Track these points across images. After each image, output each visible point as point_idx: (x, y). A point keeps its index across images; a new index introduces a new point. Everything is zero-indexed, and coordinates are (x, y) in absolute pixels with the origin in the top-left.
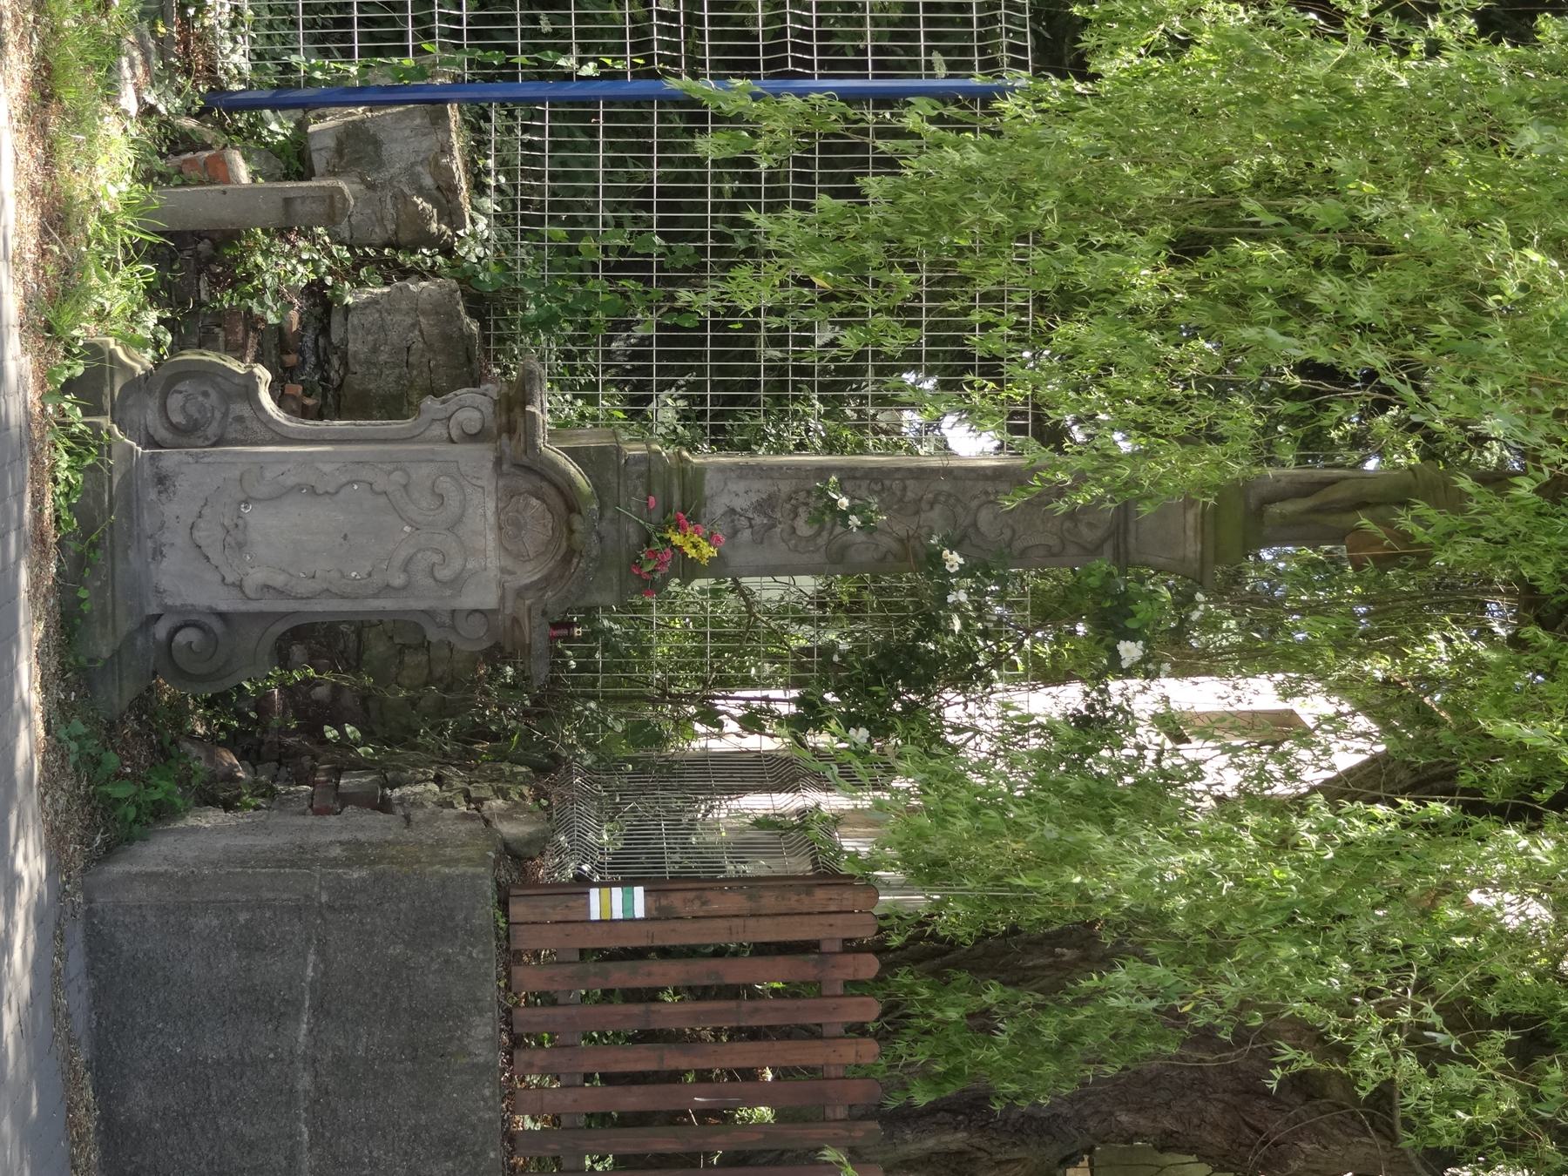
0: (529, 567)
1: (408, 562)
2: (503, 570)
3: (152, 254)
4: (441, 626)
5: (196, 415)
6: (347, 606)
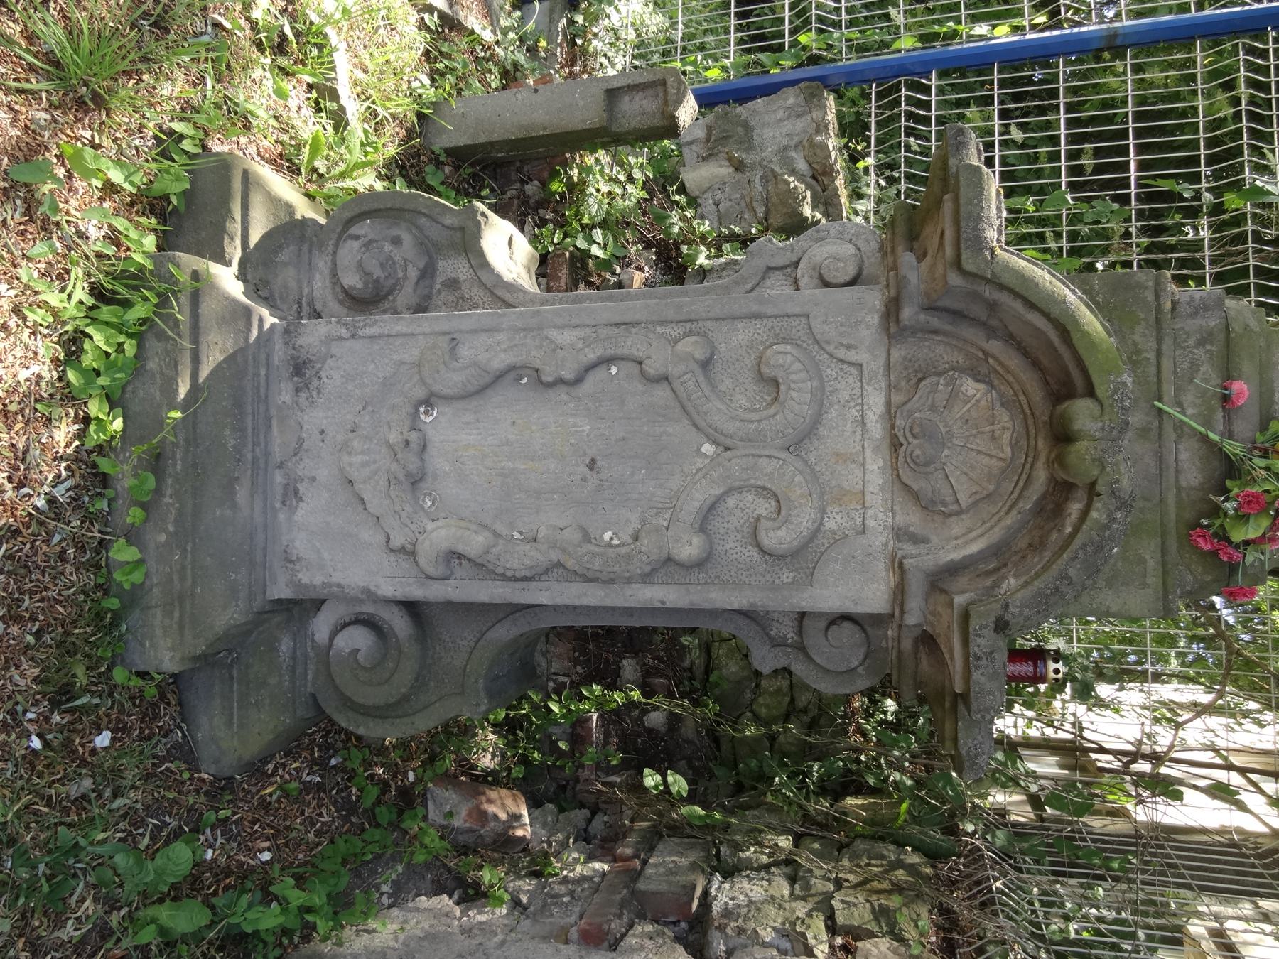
0: (956, 527)
1: (711, 509)
2: (901, 534)
4: (779, 643)
5: (378, 273)
6: (593, 596)
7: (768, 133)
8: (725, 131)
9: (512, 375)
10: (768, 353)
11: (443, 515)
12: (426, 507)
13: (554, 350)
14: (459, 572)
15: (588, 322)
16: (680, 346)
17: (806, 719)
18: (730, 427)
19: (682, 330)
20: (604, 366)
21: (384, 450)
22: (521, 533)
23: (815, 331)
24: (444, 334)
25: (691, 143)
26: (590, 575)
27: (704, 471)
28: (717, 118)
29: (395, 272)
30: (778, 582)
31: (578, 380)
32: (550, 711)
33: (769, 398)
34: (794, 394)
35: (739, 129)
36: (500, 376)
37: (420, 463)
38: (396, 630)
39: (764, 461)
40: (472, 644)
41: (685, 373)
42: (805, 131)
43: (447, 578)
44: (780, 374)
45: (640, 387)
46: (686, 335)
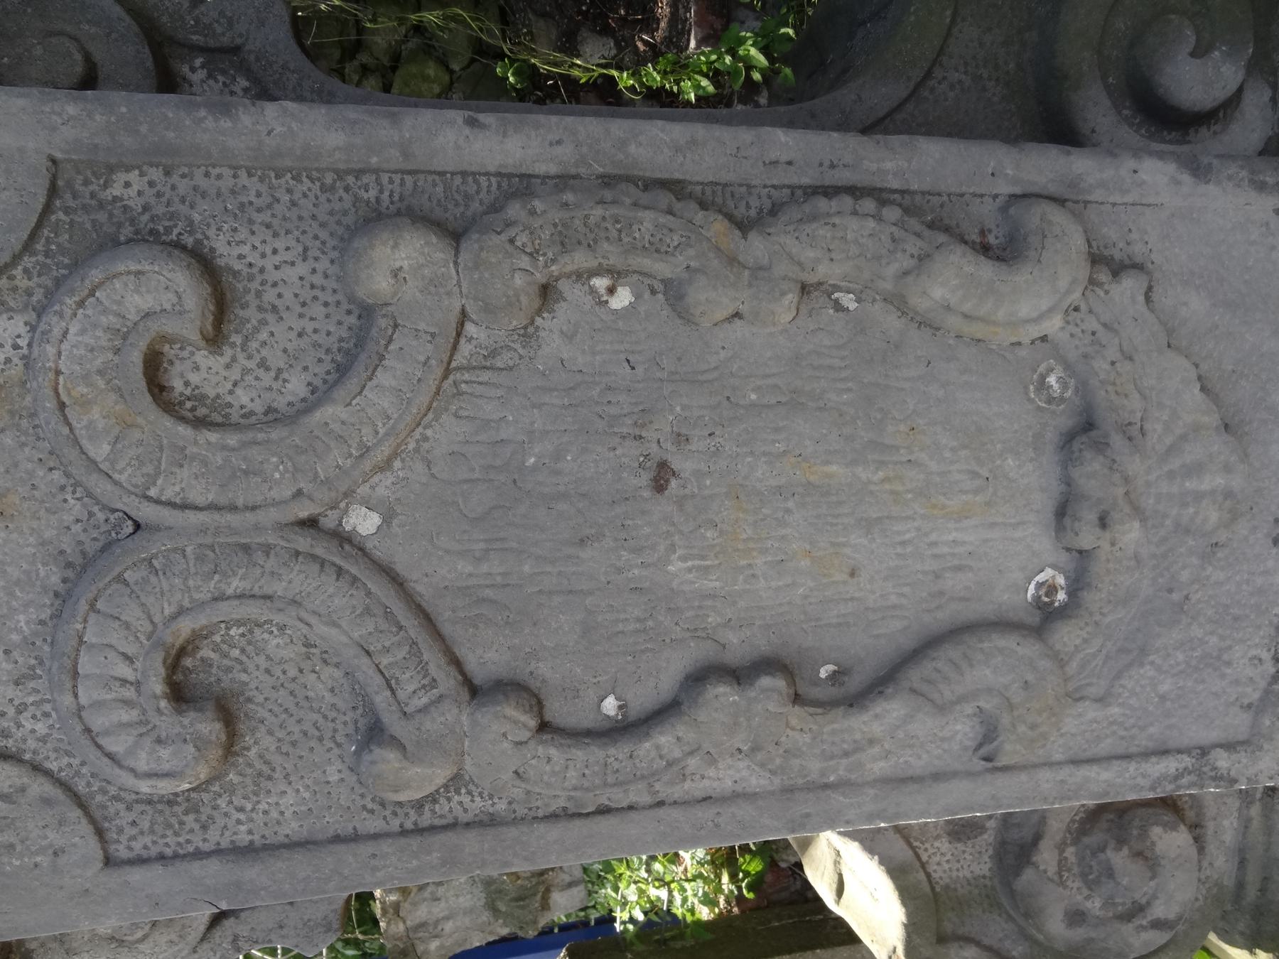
1: (349, 360)
3: (505, 135)
5: (1119, 858)
7: (465, 901)
8: (523, 907)
9: (855, 683)
10: (203, 772)
11: (1023, 353)
12: (1059, 371)
13: (755, 749)
14: (986, 211)
15: (675, 813)
16: (441, 775)
17: (364, 58)
18: (297, 580)
19: (443, 807)
20: (633, 714)
21: (1149, 503)
22: (838, 307)
23: (85, 828)
24: (1005, 769)
25: (570, 885)
26: (665, 198)
27: (367, 465)
28: (535, 922)
29: (1081, 859)
30: (155, 174)
31: (699, 678)
32: (765, 50)
33: (206, 652)
34: (124, 671)
35: (503, 909)
36: (884, 681)
37: (1076, 473)
38: (1108, 103)
39: (198, 495)
40: (938, 73)
41: (424, 710)
42: (414, 904)
43: (1014, 197)
44: (168, 721)
45: (544, 669)
46: (433, 798)
